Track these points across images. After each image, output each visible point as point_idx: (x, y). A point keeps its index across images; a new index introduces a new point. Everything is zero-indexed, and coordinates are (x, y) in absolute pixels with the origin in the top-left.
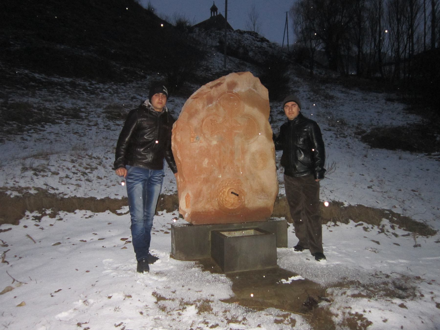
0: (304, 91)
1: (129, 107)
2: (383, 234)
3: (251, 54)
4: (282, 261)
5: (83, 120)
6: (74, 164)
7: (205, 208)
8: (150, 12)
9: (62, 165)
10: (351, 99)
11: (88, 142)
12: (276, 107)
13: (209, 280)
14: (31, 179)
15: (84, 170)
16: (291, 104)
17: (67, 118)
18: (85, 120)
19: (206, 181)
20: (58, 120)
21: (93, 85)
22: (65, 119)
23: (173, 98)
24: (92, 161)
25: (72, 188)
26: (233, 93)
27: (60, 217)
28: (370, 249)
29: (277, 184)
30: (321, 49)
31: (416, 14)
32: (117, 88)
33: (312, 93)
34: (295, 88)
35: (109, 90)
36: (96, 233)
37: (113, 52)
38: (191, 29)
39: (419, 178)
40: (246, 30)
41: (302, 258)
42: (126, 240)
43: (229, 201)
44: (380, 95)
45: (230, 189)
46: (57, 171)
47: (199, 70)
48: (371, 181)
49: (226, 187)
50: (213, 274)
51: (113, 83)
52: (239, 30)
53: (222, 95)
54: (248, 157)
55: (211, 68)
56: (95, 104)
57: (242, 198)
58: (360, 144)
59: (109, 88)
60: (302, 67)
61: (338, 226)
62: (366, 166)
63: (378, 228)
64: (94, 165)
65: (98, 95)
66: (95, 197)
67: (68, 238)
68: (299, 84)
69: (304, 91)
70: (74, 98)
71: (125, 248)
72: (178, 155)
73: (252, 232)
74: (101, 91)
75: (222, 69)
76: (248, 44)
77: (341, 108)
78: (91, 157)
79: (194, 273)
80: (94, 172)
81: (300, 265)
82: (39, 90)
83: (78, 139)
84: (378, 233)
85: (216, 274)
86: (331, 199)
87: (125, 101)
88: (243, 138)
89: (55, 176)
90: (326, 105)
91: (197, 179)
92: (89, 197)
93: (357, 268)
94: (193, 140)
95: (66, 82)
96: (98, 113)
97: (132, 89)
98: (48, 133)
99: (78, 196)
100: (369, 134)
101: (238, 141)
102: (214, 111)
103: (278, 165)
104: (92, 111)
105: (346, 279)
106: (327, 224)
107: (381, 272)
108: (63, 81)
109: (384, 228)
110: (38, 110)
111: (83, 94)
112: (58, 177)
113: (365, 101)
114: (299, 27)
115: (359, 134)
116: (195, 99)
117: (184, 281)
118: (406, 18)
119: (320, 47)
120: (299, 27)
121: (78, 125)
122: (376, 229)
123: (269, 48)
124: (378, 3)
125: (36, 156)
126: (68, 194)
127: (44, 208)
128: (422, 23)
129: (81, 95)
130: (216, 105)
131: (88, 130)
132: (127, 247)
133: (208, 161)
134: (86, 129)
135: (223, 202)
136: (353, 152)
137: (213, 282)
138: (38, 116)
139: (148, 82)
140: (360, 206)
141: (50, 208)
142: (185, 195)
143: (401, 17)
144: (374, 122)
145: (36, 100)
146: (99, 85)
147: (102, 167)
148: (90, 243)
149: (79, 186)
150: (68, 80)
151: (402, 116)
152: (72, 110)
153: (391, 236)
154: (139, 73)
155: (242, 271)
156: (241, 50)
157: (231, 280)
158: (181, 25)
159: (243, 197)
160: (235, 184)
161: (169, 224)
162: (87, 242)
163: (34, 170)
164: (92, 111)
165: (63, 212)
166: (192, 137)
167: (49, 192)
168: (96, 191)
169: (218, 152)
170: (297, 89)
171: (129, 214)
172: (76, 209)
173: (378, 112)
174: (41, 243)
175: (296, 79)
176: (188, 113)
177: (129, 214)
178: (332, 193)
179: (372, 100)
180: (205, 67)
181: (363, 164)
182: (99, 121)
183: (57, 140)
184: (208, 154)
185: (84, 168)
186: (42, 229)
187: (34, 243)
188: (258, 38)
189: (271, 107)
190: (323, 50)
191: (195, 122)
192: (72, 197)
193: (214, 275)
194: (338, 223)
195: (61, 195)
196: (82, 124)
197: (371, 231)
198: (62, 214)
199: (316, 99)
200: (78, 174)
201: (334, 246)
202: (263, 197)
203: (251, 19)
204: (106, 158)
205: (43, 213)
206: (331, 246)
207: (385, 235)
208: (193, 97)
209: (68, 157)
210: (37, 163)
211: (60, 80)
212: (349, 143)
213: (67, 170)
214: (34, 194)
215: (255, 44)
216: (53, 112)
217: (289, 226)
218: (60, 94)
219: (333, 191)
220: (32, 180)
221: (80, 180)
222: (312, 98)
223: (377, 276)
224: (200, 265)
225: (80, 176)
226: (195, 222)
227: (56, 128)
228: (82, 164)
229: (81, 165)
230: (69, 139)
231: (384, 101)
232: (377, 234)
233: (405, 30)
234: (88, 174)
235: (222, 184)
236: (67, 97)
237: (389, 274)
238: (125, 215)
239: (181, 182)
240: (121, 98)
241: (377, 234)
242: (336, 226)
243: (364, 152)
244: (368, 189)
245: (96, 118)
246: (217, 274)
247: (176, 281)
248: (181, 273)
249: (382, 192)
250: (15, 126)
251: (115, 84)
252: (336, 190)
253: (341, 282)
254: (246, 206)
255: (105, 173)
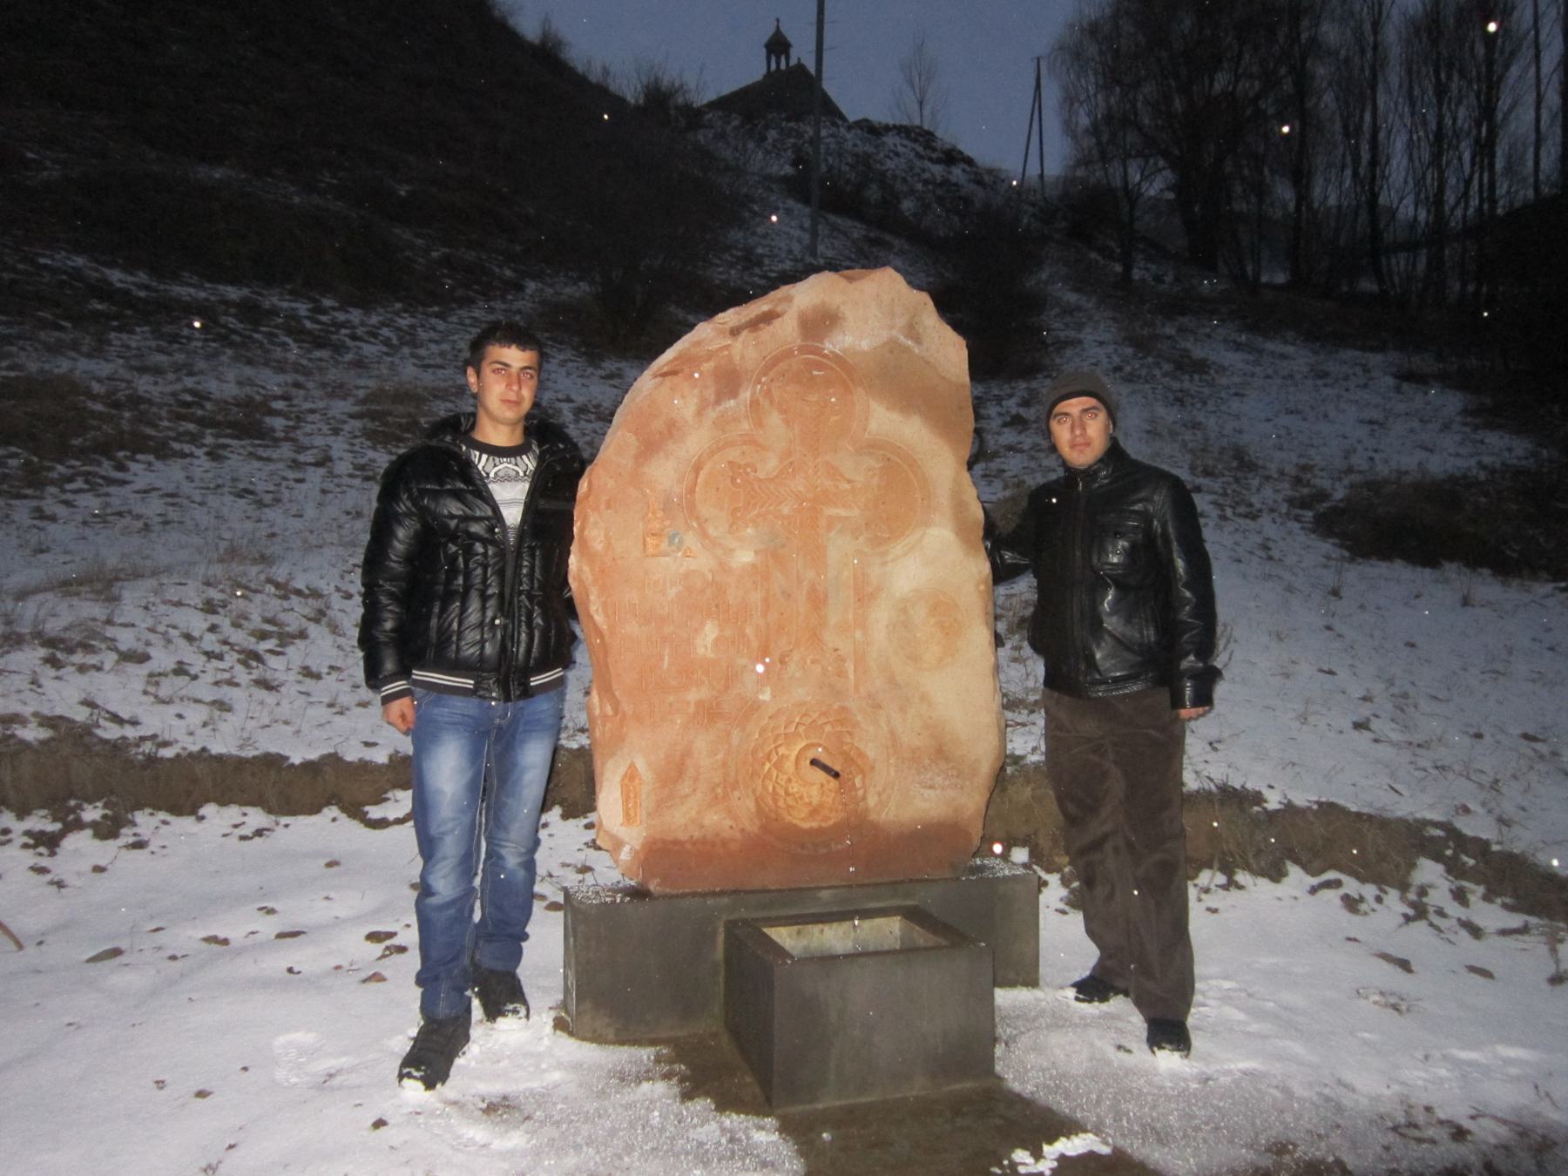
0: (1101, 343)
1: (453, 394)
2: (1421, 925)
3: (907, 205)
4: (1017, 1051)
5: (276, 442)
6: (215, 619)
7: (702, 827)
8: (547, 55)
9: (166, 621)
10: (1270, 371)
11: (286, 530)
12: (999, 400)
13: (707, 1151)
14: (32, 683)
15: (251, 643)
16: (1080, 408)
17: (217, 436)
18: (283, 443)
19: (709, 713)
20: (181, 442)
21: (324, 312)
22: (209, 440)
23: (617, 365)
24: (286, 604)
25: (196, 715)
26: (825, 356)
27: (135, 835)
28: (1377, 998)
29: (999, 725)
30: (1161, 190)
31: (1507, 67)
32: (412, 327)
33: (1129, 351)
34: (1067, 333)
35: (385, 332)
36: (270, 905)
37: (403, 193)
38: (694, 116)
39: (1545, 685)
40: (891, 122)
41: (1098, 1043)
42: (388, 943)
43: (801, 798)
44: (1375, 359)
45: (808, 747)
46: (140, 648)
47: (718, 262)
48: (1365, 699)
49: (789, 739)
50: (723, 1118)
51: (399, 306)
52: (866, 120)
53: (776, 361)
54: (881, 616)
55: (763, 256)
56: (324, 385)
57: (854, 784)
58: (1309, 543)
59: (383, 324)
60: (1093, 255)
61: (1240, 887)
62: (1339, 636)
63: (1403, 899)
64: (293, 622)
65: (339, 349)
66: (282, 752)
67: (157, 930)
68: (1081, 315)
69: (1101, 343)
70: (250, 362)
71: (377, 977)
72: (593, 608)
73: (888, 930)
74: (354, 338)
75: (802, 260)
76: (898, 172)
77: (1235, 405)
78: (285, 591)
79: (648, 1108)
80: (290, 650)
81: (1092, 1078)
82: (119, 330)
83: (248, 518)
84: (1402, 920)
85: (738, 1113)
86: (1212, 776)
87: (440, 372)
88: (861, 539)
89: (132, 668)
90: (1180, 395)
91: (671, 704)
92: (256, 753)
93: (1327, 1091)
94: (658, 545)
95: (227, 303)
96: (334, 418)
97: (470, 329)
98: (137, 492)
99: (217, 748)
100: (1341, 505)
101: (841, 550)
102: (745, 426)
103: (1002, 627)
104: (312, 411)
105: (1288, 1152)
106: (1196, 881)
107: (1428, 1109)
108: (213, 298)
109: (1425, 900)
110: (105, 404)
111: (284, 345)
112: (143, 670)
113: (1320, 382)
114: (1082, 112)
115: (1304, 504)
116: (669, 380)
117: (598, 1152)
118: (1470, 83)
119: (1157, 185)
120: (1082, 112)
121: (257, 464)
122: (1395, 903)
123: (973, 187)
124: (1368, 27)
125: (67, 587)
126: (177, 741)
127: (76, 797)
128: (1530, 98)
129: (279, 349)
130: (755, 404)
131: (292, 484)
132: (385, 973)
133: (717, 632)
134: (285, 479)
135: (775, 801)
136: (1287, 576)
137: (719, 1160)
138: (104, 427)
139: (530, 305)
140: (1328, 810)
141: (99, 799)
142: (622, 770)
143: (1449, 78)
144: (1359, 461)
145: (104, 369)
146: (348, 312)
147: (326, 631)
148: (241, 951)
149: (222, 706)
150: (233, 293)
151: (1458, 438)
152: (238, 405)
153: (1456, 933)
154: (497, 270)
155: (851, 1101)
156: (873, 193)
157: (802, 1153)
158: (659, 99)
159: (858, 781)
160: (828, 728)
161: (568, 865)
162: (233, 944)
163: (51, 643)
164: (312, 411)
165: (152, 814)
166: (653, 535)
167: (99, 732)
168: (289, 729)
169: (756, 597)
170: (1072, 334)
171: (411, 823)
172: (207, 801)
173: (1371, 422)
174: (43, 947)
175: (1072, 298)
176: (636, 434)
177: (411, 823)
178: (1215, 749)
179: (1346, 378)
180: (739, 254)
181: (1329, 628)
182: (335, 446)
183: (169, 518)
184: (717, 606)
185: (253, 634)
186: (60, 884)
187: (13, 947)
188: (934, 150)
189: (978, 404)
190: (1170, 196)
191: (665, 473)
192: (191, 755)
193: (733, 1120)
194: (1242, 877)
195: (147, 747)
196: (269, 460)
197: (1373, 910)
198: (145, 822)
199: (1144, 372)
200: (227, 657)
201: (1226, 978)
202: (939, 780)
203: (913, 86)
204: (345, 592)
205: (71, 817)
206: (1217, 978)
207: (1430, 929)
208: (659, 369)
209: (193, 593)
210: (63, 615)
211: (203, 295)
212: (1268, 539)
213: (183, 643)
214: (35, 743)
215: (924, 170)
216: (164, 413)
217: (1045, 884)
218: (200, 344)
219: (1219, 742)
220: (34, 687)
221: (232, 683)
222: (1128, 369)
223: (1416, 1133)
224: (676, 1067)
225: (232, 668)
226: (659, 885)
227: (170, 474)
228: (247, 619)
229: (243, 622)
230: (217, 517)
231: (1390, 381)
232: (1400, 926)
233: (1466, 126)
234: (267, 657)
235: (773, 730)
236: (224, 358)
237: (1467, 1124)
238: (396, 827)
239: (604, 716)
240: (427, 362)
241: (1400, 926)
242: (1232, 889)
243: (1329, 578)
244: (1356, 734)
245: (326, 435)
246: (742, 1116)
247: (566, 1154)
248: (591, 1106)
249: (1410, 744)
250: (13, 462)
251: (406, 311)
252: (1230, 736)
253: (1268, 1168)
254: (873, 817)
255: (335, 652)
